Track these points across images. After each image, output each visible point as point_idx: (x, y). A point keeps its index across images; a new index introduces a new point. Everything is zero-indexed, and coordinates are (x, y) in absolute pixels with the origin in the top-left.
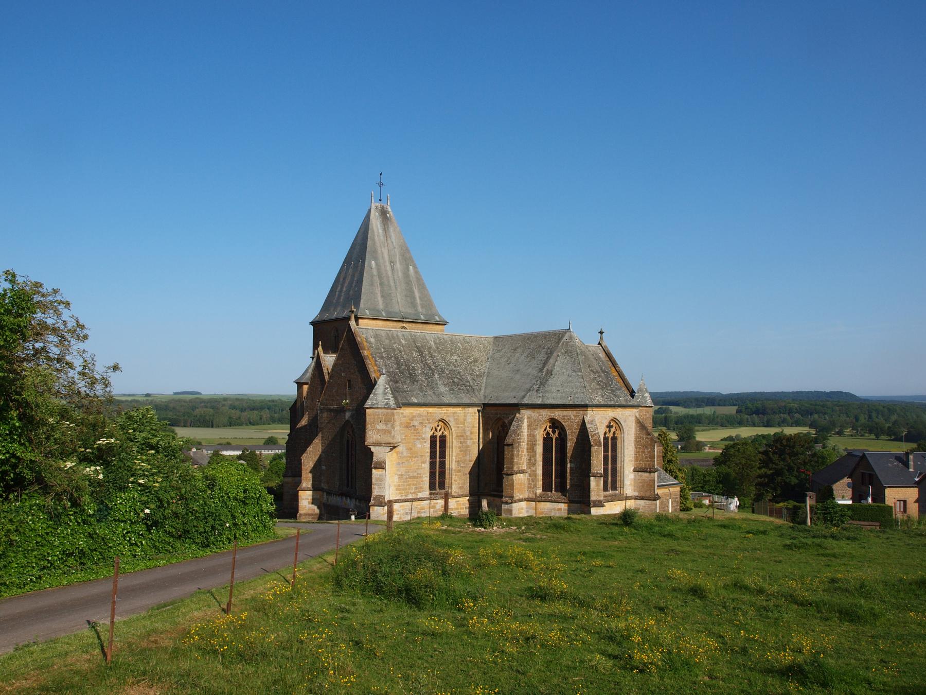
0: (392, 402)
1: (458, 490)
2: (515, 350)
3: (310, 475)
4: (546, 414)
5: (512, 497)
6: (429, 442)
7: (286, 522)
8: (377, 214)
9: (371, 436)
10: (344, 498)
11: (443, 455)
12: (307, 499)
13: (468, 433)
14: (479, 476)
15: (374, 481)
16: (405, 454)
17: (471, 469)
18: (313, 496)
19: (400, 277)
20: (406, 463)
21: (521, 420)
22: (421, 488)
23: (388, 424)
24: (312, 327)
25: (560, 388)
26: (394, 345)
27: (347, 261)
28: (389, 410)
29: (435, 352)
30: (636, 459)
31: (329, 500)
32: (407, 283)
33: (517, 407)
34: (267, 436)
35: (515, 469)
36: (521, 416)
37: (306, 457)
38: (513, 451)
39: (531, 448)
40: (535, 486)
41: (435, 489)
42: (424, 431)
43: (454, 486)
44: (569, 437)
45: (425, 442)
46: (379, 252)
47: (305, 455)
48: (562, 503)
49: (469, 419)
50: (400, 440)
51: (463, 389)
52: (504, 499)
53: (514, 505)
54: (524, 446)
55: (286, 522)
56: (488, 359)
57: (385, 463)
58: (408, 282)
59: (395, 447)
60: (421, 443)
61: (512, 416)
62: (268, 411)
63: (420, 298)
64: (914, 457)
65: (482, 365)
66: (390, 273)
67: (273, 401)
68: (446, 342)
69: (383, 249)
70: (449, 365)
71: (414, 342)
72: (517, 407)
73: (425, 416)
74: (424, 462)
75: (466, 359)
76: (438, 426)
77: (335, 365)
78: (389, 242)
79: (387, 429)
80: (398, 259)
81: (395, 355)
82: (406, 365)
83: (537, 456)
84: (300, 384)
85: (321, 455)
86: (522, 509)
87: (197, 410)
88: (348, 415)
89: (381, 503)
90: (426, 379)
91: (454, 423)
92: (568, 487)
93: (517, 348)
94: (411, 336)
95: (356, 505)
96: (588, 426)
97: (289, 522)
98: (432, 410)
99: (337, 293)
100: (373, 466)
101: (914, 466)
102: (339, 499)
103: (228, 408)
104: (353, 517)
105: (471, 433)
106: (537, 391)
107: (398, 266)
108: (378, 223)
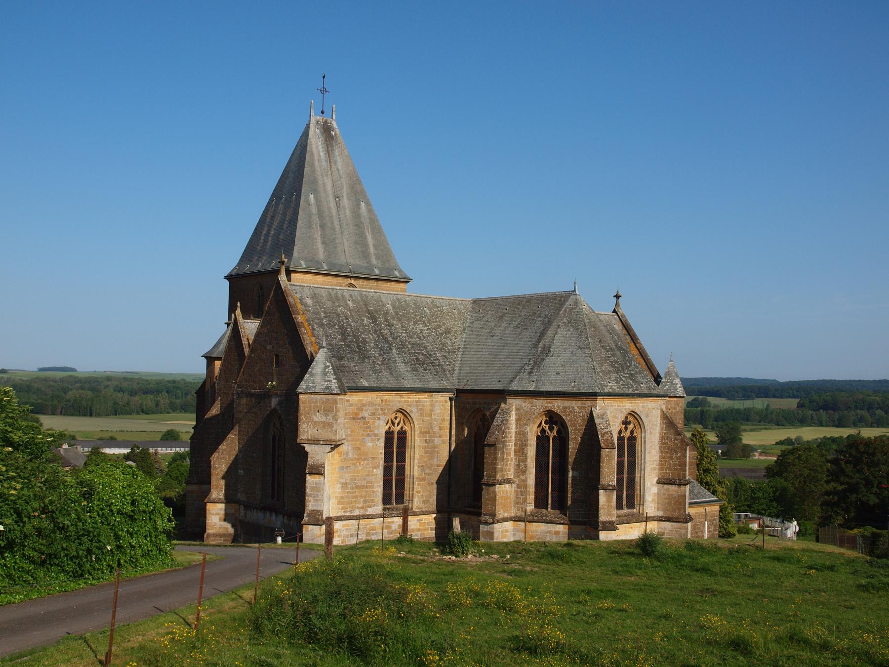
0: (334, 386)
1: (421, 505)
2: (501, 318)
3: (223, 482)
4: (541, 404)
5: (493, 515)
6: (383, 440)
7: (189, 545)
8: (318, 131)
9: (306, 431)
11: (402, 457)
15: (308, 491)
16: (351, 456)
17: (439, 477)
21: (507, 412)
22: (372, 501)
23: (328, 415)
25: (560, 369)
26: (339, 309)
27: (277, 194)
28: (330, 397)
29: (394, 320)
30: (662, 466)
33: (502, 395)
34: (165, 429)
36: (507, 407)
37: (217, 458)
38: (495, 454)
39: (521, 450)
40: (525, 500)
41: (391, 503)
42: (376, 424)
43: (415, 500)
44: (571, 436)
45: (378, 440)
46: (320, 182)
48: (560, 524)
49: (438, 410)
50: (344, 437)
51: (430, 370)
53: (496, 525)
54: (511, 446)
56: (464, 329)
57: (324, 467)
58: (359, 225)
59: (337, 446)
60: (373, 441)
61: (496, 407)
62: (166, 394)
63: (374, 246)
65: (456, 338)
66: (334, 211)
67: (174, 382)
68: (408, 305)
69: (325, 178)
70: (411, 337)
72: (502, 395)
73: (379, 405)
74: (376, 467)
75: (434, 329)
76: (396, 418)
77: (258, 335)
78: (334, 168)
79: (328, 421)
81: (339, 322)
82: (354, 336)
83: (529, 460)
84: (210, 359)
85: (237, 455)
87: (70, 393)
88: (274, 401)
89: (318, 520)
90: (381, 355)
92: (569, 503)
93: (504, 315)
94: (362, 297)
95: (283, 522)
96: (597, 421)
98: (388, 396)
99: (263, 237)
102: (261, 514)
103: (112, 390)
104: (279, 539)
105: (440, 429)
106: (530, 373)
107: (345, 202)
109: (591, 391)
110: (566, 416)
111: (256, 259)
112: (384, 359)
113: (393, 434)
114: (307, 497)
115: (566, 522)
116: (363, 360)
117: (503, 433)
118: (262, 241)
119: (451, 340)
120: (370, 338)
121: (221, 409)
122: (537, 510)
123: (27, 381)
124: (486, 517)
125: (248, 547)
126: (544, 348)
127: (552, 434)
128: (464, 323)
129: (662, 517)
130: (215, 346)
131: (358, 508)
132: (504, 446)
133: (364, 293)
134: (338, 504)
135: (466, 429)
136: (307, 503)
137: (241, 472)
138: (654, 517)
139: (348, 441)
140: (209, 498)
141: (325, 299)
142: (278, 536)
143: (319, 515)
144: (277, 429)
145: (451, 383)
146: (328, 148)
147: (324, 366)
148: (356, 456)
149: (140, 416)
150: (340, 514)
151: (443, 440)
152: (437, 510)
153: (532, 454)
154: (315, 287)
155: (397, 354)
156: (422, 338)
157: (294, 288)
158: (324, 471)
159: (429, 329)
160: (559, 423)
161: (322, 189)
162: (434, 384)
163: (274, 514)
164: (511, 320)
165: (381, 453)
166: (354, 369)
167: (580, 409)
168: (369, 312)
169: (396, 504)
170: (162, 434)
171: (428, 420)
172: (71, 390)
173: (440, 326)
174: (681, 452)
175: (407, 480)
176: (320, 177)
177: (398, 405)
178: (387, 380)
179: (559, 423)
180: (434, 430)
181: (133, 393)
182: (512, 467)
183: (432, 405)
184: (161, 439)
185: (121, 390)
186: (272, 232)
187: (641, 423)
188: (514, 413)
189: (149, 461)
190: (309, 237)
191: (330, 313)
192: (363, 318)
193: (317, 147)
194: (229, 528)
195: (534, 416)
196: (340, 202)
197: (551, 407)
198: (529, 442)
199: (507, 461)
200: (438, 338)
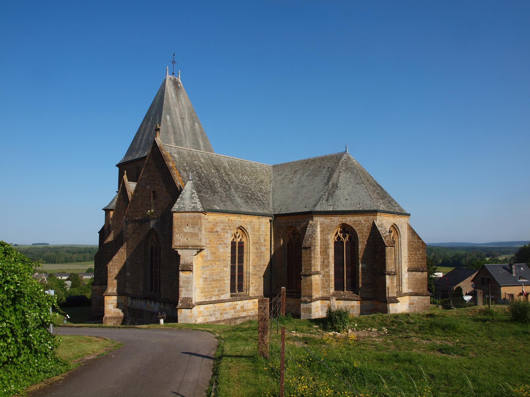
0: (199, 206)
1: (254, 292)
2: (295, 172)
3: (115, 282)
4: (337, 220)
5: (310, 296)
6: (230, 247)
7: (91, 327)
8: (171, 83)
9: (178, 239)
10: (148, 302)
11: (241, 261)
12: (113, 303)
13: (262, 241)
14: (271, 280)
15: (181, 283)
16: (209, 258)
17: (265, 273)
18: (118, 300)
19: (189, 130)
20: (210, 266)
21: (315, 226)
22: (224, 290)
23: (195, 228)
24: (118, 169)
25: (347, 197)
26: (195, 162)
27: (147, 118)
28: (196, 214)
29: (230, 172)
30: (410, 260)
31: (134, 304)
32: (193, 134)
33: (310, 214)
34: (87, 268)
35: (313, 270)
36: (314, 223)
37: (112, 265)
38: (310, 254)
39: (324, 251)
40: (329, 286)
41: (235, 292)
42: (226, 236)
43: (251, 289)
44: (360, 240)
45: (227, 247)
46: (173, 110)
47: (111, 263)
48: (355, 300)
49: (263, 228)
50: (205, 245)
51: (255, 203)
52: (303, 299)
53: (313, 303)
54: (318, 249)
55: (91, 327)
56: (271, 181)
57: (192, 266)
58: (195, 134)
59: (201, 250)
60: (223, 248)
61: (305, 224)
62: (89, 254)
63: (204, 146)
64: (515, 267)
65: (267, 186)
66: (181, 126)
67: (92, 248)
68: (237, 165)
69: (175, 108)
70: (241, 183)
71: (212, 162)
72: (310, 214)
73: (227, 223)
74: (226, 266)
75: (254, 179)
76: (237, 233)
77: (136, 191)
78: (180, 103)
79: (195, 232)
80: (186, 116)
81: (197, 170)
82: (207, 179)
83: (330, 258)
84: (107, 211)
85: (125, 263)
86: (318, 307)
87: (46, 253)
88: (152, 223)
89: (189, 305)
90: (225, 192)
91: (251, 230)
92: (360, 286)
93: (297, 170)
94: (209, 157)
95: (160, 307)
96: (379, 229)
97: (94, 327)
98: (233, 217)
99: (139, 141)
100: (180, 269)
101: (516, 272)
102: (143, 303)
103: (64, 252)
104: (162, 321)
105: (265, 240)
106: (327, 200)
107: (187, 121)
108: (172, 89)
109: (372, 209)
110: (356, 227)
111: (134, 153)
112: (227, 194)
113: (236, 244)
114: (180, 288)
115: (359, 299)
116: (214, 194)
117: (314, 240)
118: (138, 143)
119: (264, 187)
120: (217, 181)
121: (114, 238)
122: (336, 292)
123: (27, 249)
124: (305, 298)
125: (137, 328)
126: (333, 185)
127: (345, 240)
128: (270, 178)
129: (412, 293)
130: (110, 203)
131: (214, 295)
132: (315, 248)
133: (210, 155)
134: (201, 293)
135: (282, 240)
136: (180, 293)
137: (128, 274)
138: (407, 293)
139: (207, 248)
140: (106, 293)
141: (186, 155)
142: (160, 318)
143: (189, 301)
144: (154, 242)
145: (270, 211)
146: (176, 92)
147: (191, 193)
148: (213, 259)
149: (76, 263)
150: (203, 300)
151: (266, 248)
152: (264, 295)
153: (332, 255)
154: (179, 148)
155: (234, 192)
156: (248, 184)
157: (165, 147)
158: (193, 268)
159: (251, 179)
160: (350, 232)
161: (174, 114)
162: (259, 211)
163: (153, 301)
164: (303, 173)
165: (229, 257)
166: (209, 199)
167: (365, 222)
168: (214, 166)
169: (239, 292)
170: (86, 270)
171: (257, 235)
172: (46, 252)
173: (257, 178)
174: (422, 250)
175: (245, 275)
176: (172, 107)
177: (239, 224)
178: (230, 207)
179: (350, 232)
180: (261, 242)
181: (74, 253)
182: (319, 263)
183: (260, 225)
184: (86, 272)
185: (69, 252)
186: (145, 137)
187: (398, 232)
188: (319, 226)
189: (78, 280)
190: (167, 138)
191: (190, 164)
192: (211, 169)
193: (171, 91)
194: (120, 313)
195: (333, 228)
196: (184, 121)
197: (345, 221)
198: (330, 246)
199: (317, 259)
200: (257, 185)
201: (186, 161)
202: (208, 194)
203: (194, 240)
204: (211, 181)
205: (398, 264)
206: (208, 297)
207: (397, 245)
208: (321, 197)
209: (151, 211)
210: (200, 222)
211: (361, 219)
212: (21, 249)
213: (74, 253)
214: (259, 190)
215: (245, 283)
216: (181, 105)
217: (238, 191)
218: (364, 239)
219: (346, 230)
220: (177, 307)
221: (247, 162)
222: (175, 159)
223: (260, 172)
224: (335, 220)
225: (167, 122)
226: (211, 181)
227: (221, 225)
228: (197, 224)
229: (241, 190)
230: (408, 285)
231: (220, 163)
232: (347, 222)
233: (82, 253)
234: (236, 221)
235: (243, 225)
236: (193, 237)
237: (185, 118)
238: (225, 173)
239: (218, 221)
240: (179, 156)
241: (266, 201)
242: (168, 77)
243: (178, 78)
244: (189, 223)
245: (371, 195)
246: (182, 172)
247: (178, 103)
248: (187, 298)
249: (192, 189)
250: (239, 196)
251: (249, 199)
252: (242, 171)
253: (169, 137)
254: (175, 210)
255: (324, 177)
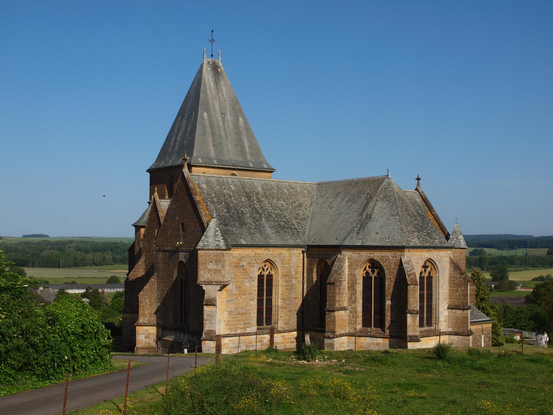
0: (222, 244)
1: (283, 326)
2: (337, 195)
4: (365, 255)
5: (334, 332)
6: (256, 281)
8: (209, 69)
9: (203, 275)
13: (293, 273)
15: (205, 317)
16: (234, 292)
19: (231, 128)
21: (342, 261)
22: (250, 323)
25: (379, 230)
26: (225, 191)
27: (181, 113)
28: (219, 252)
29: (263, 198)
30: (451, 297)
33: (338, 249)
34: (109, 276)
35: (337, 306)
36: (342, 257)
37: (143, 295)
38: (334, 289)
39: (352, 287)
41: (262, 325)
42: (252, 270)
43: (280, 322)
44: (387, 276)
45: (253, 281)
46: (211, 104)
47: (142, 293)
48: (380, 337)
49: (294, 260)
50: (229, 279)
51: (288, 232)
52: (326, 334)
53: (336, 339)
54: (345, 284)
55: (124, 355)
56: (312, 203)
57: (216, 301)
59: (225, 286)
60: (249, 282)
62: (110, 252)
63: (249, 147)
65: (306, 209)
66: (221, 124)
67: (115, 243)
68: (273, 188)
69: (214, 101)
70: (275, 210)
72: (338, 249)
73: (253, 257)
74: (252, 300)
76: (265, 266)
78: (220, 94)
81: (225, 200)
82: (235, 209)
83: (358, 294)
93: (339, 193)
95: (189, 339)
98: (259, 251)
99: (172, 143)
100: (204, 303)
103: (73, 250)
104: (186, 351)
105: (296, 273)
106: (358, 233)
107: (229, 117)
112: (256, 225)
113: (264, 277)
114: (204, 321)
116: (242, 226)
119: (303, 211)
122: (364, 328)
123: (16, 244)
124: (329, 333)
126: (367, 216)
127: (374, 275)
128: (311, 199)
129: (451, 332)
132: (341, 284)
133: (242, 180)
136: (205, 325)
138: (446, 332)
139: (232, 282)
140: (138, 322)
141: (215, 184)
142: (184, 348)
144: (183, 274)
145: (303, 241)
147: (215, 230)
148: (238, 293)
150: (227, 333)
151: (298, 281)
154: (208, 176)
155: (265, 221)
157: (193, 177)
158: (216, 303)
163: (182, 333)
164: (344, 197)
165: (255, 290)
166: (236, 232)
168: (246, 193)
169: (267, 325)
170: (107, 279)
173: (295, 202)
175: (274, 308)
176: (211, 101)
180: (292, 274)
183: (290, 257)
184: (107, 283)
187: (435, 267)
188: (347, 261)
191: (218, 194)
192: (241, 197)
193: (209, 80)
195: (361, 263)
197: (373, 257)
198: (358, 281)
199: (343, 295)
201: (215, 191)
202: (235, 227)
203: (218, 276)
204: (240, 212)
205: (435, 301)
206: (233, 330)
207: (435, 280)
208: (353, 229)
209: (179, 243)
210: (223, 259)
211: (389, 254)
212: (6, 244)
213: (87, 252)
214: (296, 216)
215: (273, 316)
216: (222, 96)
217: (270, 220)
218: (391, 276)
219: (375, 266)
220: (201, 339)
221: (285, 183)
222: (202, 191)
223: (300, 193)
224: (363, 255)
225: (204, 122)
226: (240, 212)
227: (247, 259)
228: (220, 261)
229: (274, 218)
230: (447, 324)
231: (253, 189)
232: (375, 257)
233: (100, 251)
234: (264, 254)
235: (271, 258)
236: (216, 273)
237: (227, 113)
238: (257, 200)
239: (243, 255)
240: (207, 186)
241: (302, 229)
242: (205, 61)
243: (218, 60)
244: (213, 260)
245: (404, 228)
246: (210, 204)
247: (218, 93)
248: (211, 330)
249: (216, 227)
250: (270, 226)
251: (281, 229)
252: (278, 195)
253: (207, 140)
254: (200, 248)
255: (361, 204)
